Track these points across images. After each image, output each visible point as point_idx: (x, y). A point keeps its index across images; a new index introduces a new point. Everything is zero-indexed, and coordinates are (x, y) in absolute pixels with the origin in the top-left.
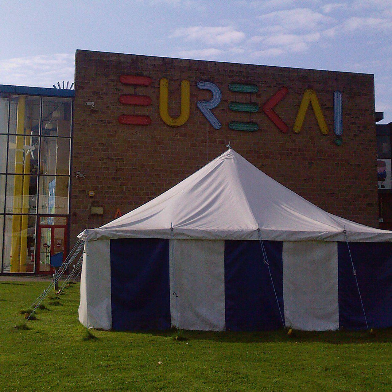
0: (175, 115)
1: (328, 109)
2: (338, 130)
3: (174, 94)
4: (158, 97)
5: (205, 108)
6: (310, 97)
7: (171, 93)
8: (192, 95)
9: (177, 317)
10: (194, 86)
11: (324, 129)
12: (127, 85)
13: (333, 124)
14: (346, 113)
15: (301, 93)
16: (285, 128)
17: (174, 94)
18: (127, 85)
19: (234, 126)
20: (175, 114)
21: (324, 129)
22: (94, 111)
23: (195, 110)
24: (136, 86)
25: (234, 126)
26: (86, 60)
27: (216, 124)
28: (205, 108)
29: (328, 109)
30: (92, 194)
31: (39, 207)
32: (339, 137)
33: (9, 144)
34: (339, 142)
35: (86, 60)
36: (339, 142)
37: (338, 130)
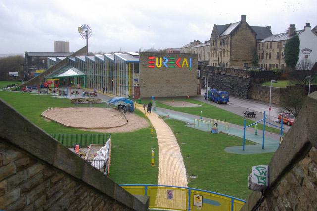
3: (159, 60)
5: (165, 63)
6: (185, 60)
15: (183, 59)
16: (181, 67)
17: (159, 60)
20: (159, 65)
22: (144, 65)
23: (163, 64)
27: (167, 67)
28: (165, 63)
29: (189, 62)
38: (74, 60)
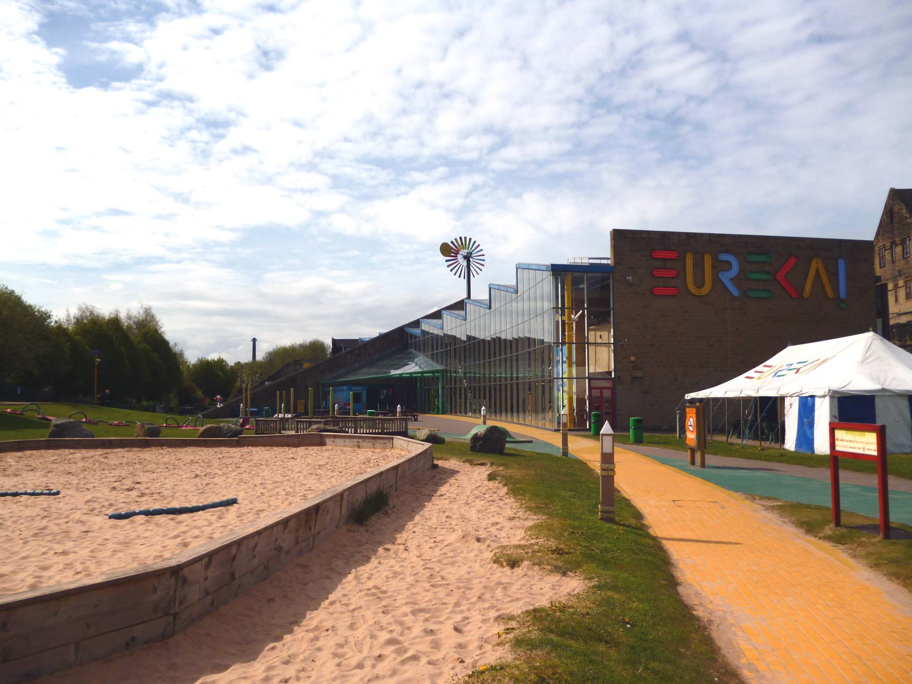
0: (700, 284)
1: (833, 275)
2: (843, 295)
3: (699, 266)
4: (685, 269)
5: (726, 277)
7: (695, 265)
8: (713, 267)
9: (611, 451)
10: (715, 259)
11: (830, 295)
12: (657, 259)
13: (838, 290)
14: (849, 278)
17: (699, 266)
18: (657, 259)
19: (752, 294)
20: (700, 284)
21: (830, 295)
22: (631, 284)
23: (716, 280)
24: (664, 260)
25: (752, 294)
26: (619, 236)
27: (736, 293)
28: (726, 277)
30: (633, 359)
31: (876, 495)
32: (842, 300)
33: (842, 484)
34: (843, 306)
35: (619, 236)
36: (843, 306)
37: (843, 295)
38: (416, 331)
